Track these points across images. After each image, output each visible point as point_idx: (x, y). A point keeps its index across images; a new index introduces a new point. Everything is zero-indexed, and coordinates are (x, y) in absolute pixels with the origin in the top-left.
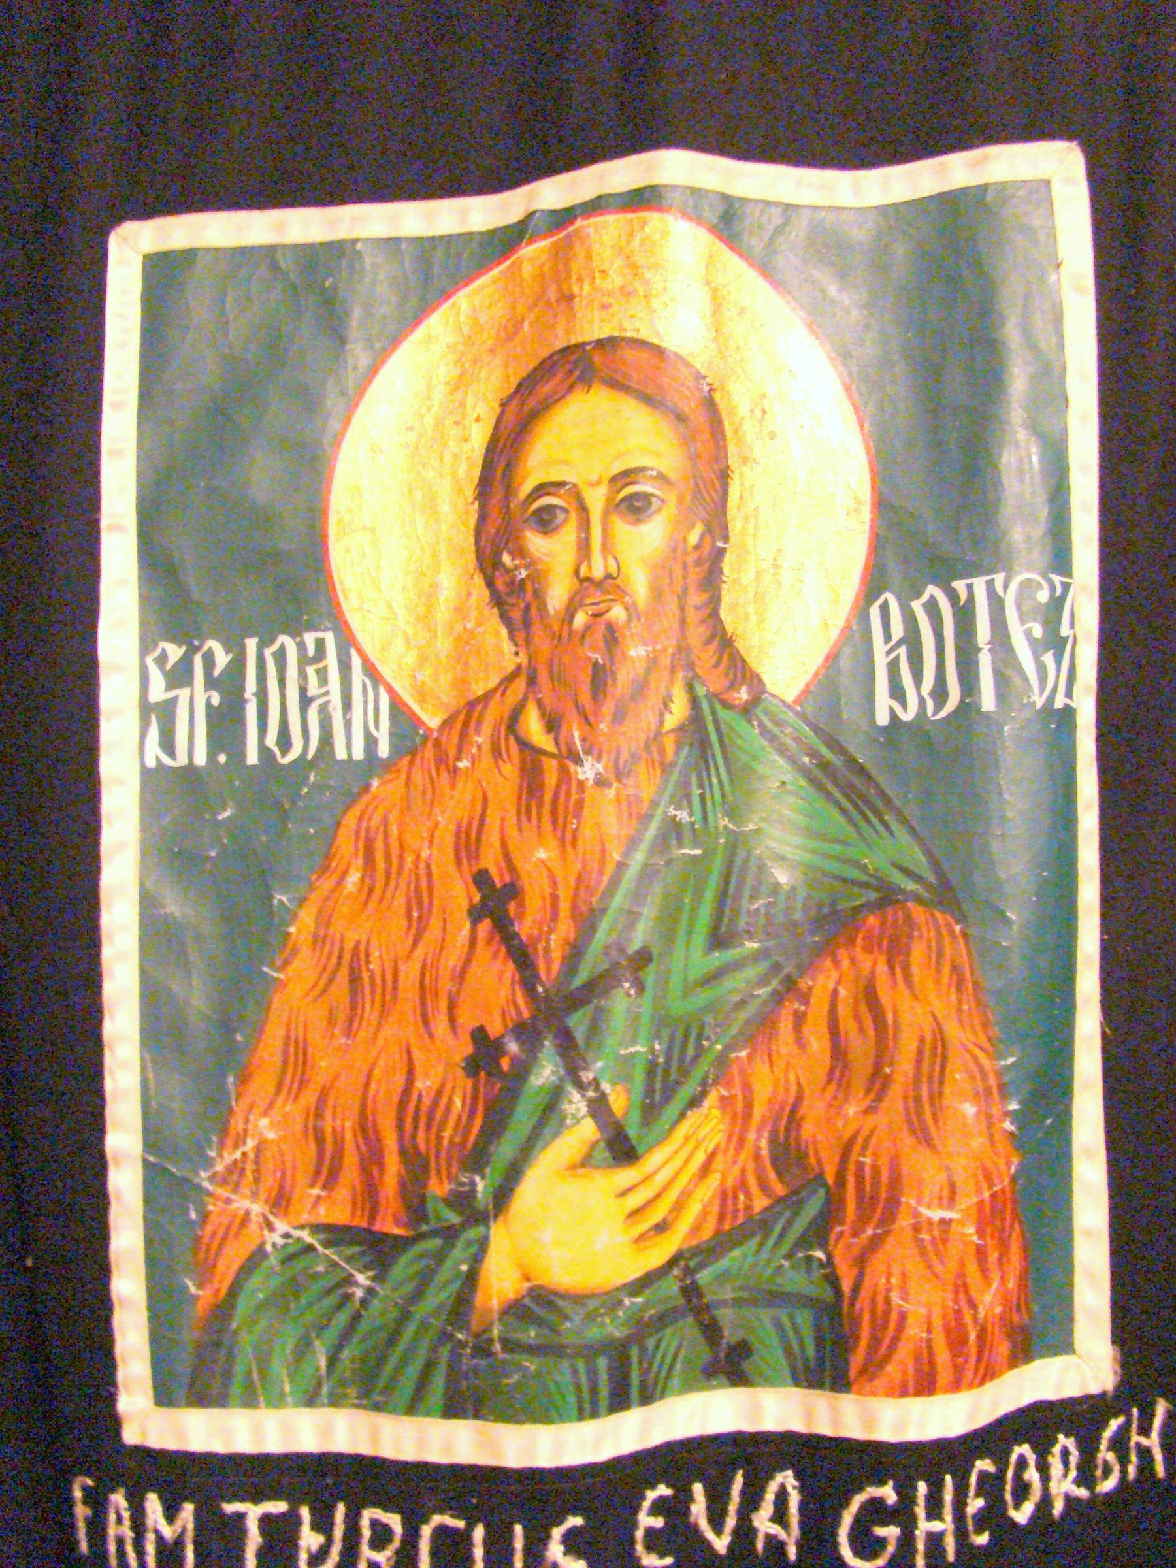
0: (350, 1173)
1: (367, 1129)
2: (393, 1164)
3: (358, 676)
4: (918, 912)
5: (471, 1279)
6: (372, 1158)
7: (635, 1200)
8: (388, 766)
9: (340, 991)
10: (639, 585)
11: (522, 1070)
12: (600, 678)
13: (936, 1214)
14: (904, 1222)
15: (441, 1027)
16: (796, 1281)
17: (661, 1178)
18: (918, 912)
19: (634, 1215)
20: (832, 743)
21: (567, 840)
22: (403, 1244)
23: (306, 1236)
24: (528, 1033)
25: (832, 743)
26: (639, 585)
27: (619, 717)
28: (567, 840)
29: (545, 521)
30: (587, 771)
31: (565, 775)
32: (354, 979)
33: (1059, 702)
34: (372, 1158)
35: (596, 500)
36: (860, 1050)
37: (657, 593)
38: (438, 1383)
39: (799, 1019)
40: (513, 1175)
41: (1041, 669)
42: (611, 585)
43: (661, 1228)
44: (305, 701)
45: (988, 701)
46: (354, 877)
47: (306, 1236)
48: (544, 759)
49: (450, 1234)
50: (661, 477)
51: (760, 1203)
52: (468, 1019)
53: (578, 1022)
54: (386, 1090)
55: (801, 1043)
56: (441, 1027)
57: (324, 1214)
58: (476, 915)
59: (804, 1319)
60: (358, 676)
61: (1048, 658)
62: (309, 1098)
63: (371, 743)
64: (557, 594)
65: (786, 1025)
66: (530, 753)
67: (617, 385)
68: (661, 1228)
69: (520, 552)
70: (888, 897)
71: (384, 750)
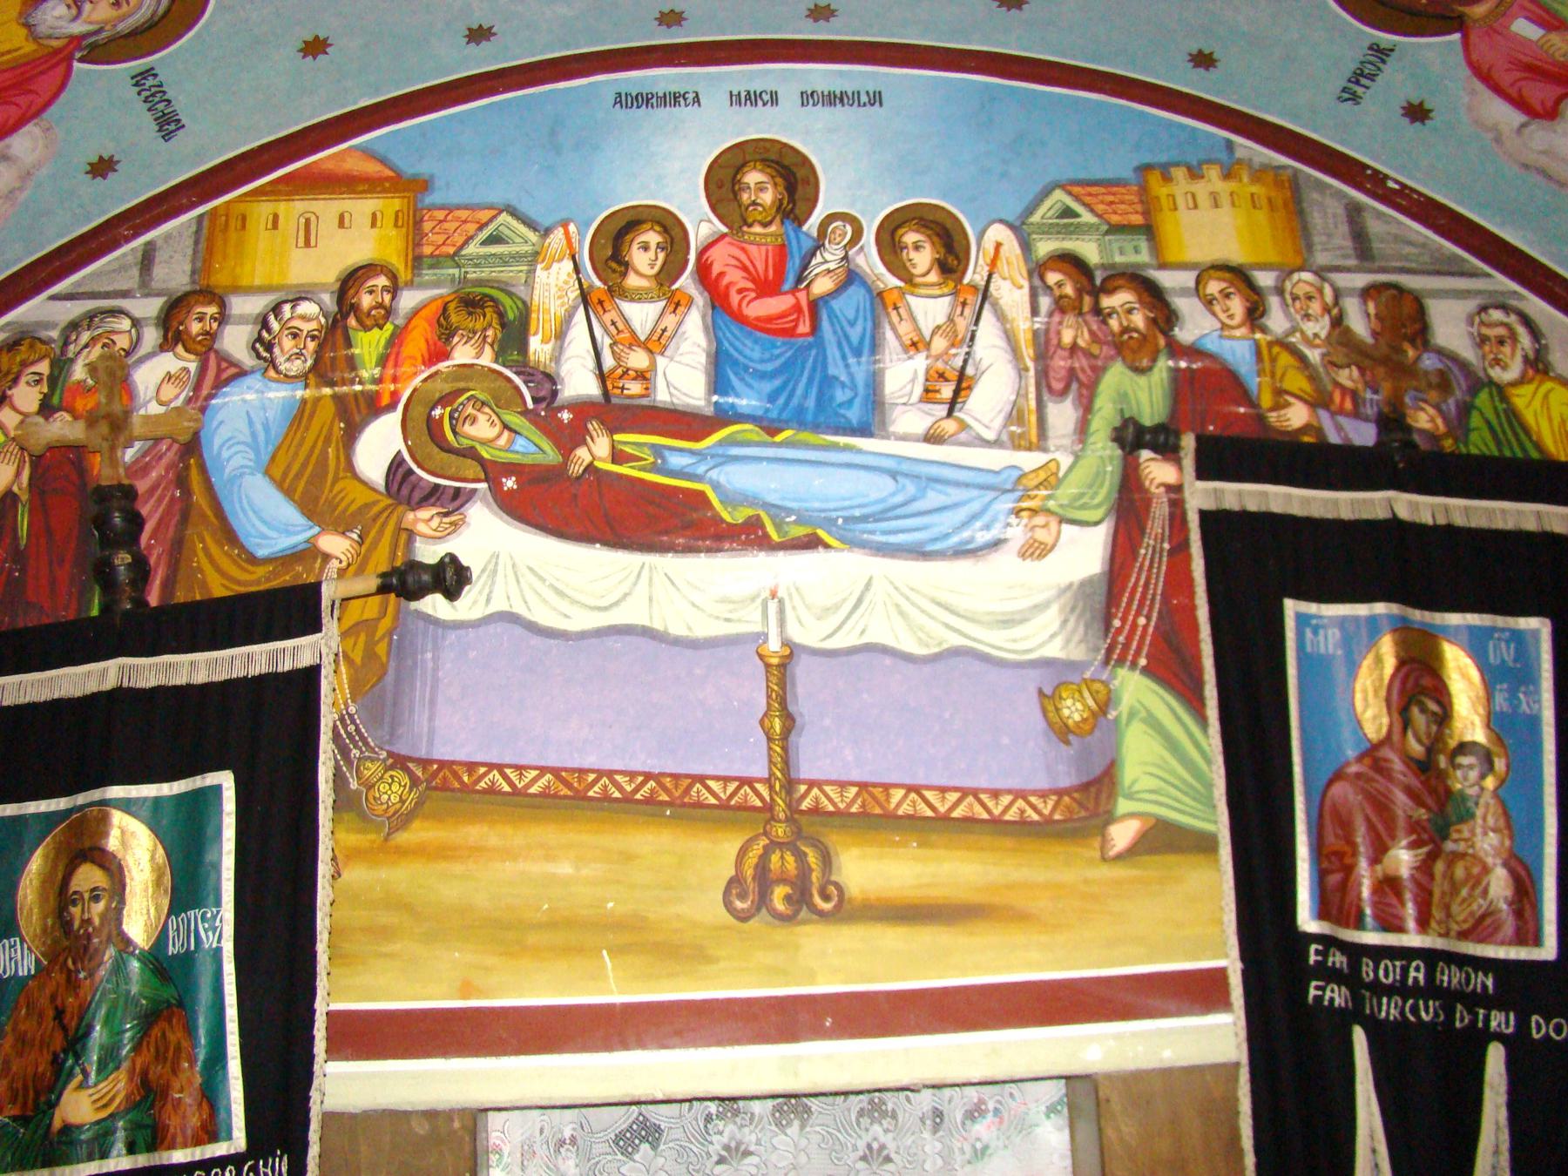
0: (20, 1099)
1: (25, 1088)
2: (31, 1095)
3: (26, 952)
4: (175, 1009)
5: (50, 1125)
6: (25, 1096)
7: (95, 1097)
8: (34, 976)
9: (20, 1045)
10: (97, 921)
11: (65, 1061)
12: (86, 948)
13: (177, 1096)
14: (169, 1099)
15: (45, 1052)
16: (148, 1121)
17: (104, 1091)
18: (175, 1009)
19: (95, 1102)
20: (157, 960)
21: (77, 995)
22: (33, 1117)
23: (7, 1120)
24: (65, 1051)
25: (157, 960)
26: (97, 921)
27: (90, 960)
28: (77, 995)
29: (74, 903)
30: (82, 975)
31: (77, 977)
32: (23, 1041)
33: (215, 945)
34: (25, 1096)
35: (86, 896)
36: (162, 1050)
37: (102, 924)
38: (40, 1158)
39: (148, 1043)
40: (60, 1094)
41: (207, 937)
42: (89, 921)
43: (105, 1106)
44: (11, 959)
45: (192, 948)
46: (23, 1012)
47: (7, 1120)
48: (1096, 842)
49: (44, 1112)
50: (104, 889)
51: (138, 1098)
52: (52, 1049)
53: (78, 1047)
54: (30, 1071)
55: (149, 1050)
56: (45, 1052)
57: (12, 1113)
58: (55, 1019)
59: (149, 1131)
60: (26, 952)
61: (210, 934)
62: (9, 1078)
63: (29, 970)
64: (76, 924)
65: (145, 1043)
66: (69, 971)
67: (93, 862)
68: (105, 1106)
69: (69, 913)
70: (170, 1005)
71: (33, 972)
